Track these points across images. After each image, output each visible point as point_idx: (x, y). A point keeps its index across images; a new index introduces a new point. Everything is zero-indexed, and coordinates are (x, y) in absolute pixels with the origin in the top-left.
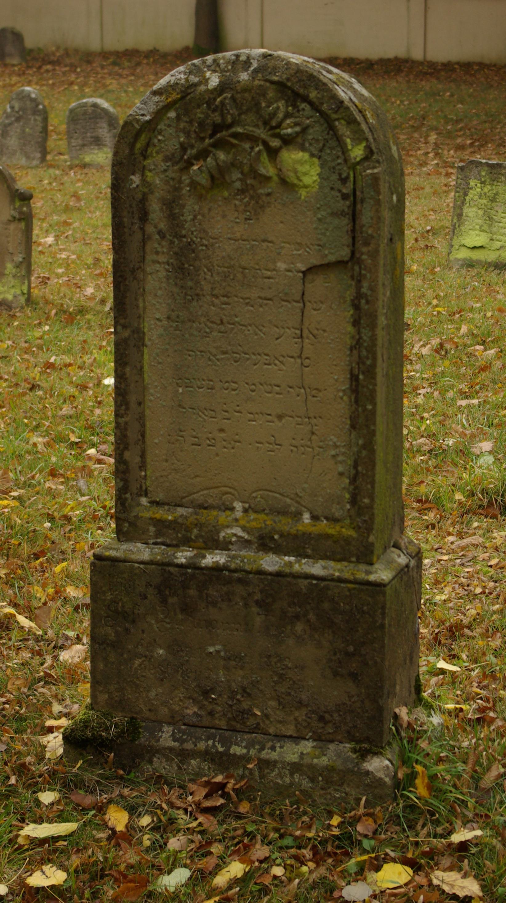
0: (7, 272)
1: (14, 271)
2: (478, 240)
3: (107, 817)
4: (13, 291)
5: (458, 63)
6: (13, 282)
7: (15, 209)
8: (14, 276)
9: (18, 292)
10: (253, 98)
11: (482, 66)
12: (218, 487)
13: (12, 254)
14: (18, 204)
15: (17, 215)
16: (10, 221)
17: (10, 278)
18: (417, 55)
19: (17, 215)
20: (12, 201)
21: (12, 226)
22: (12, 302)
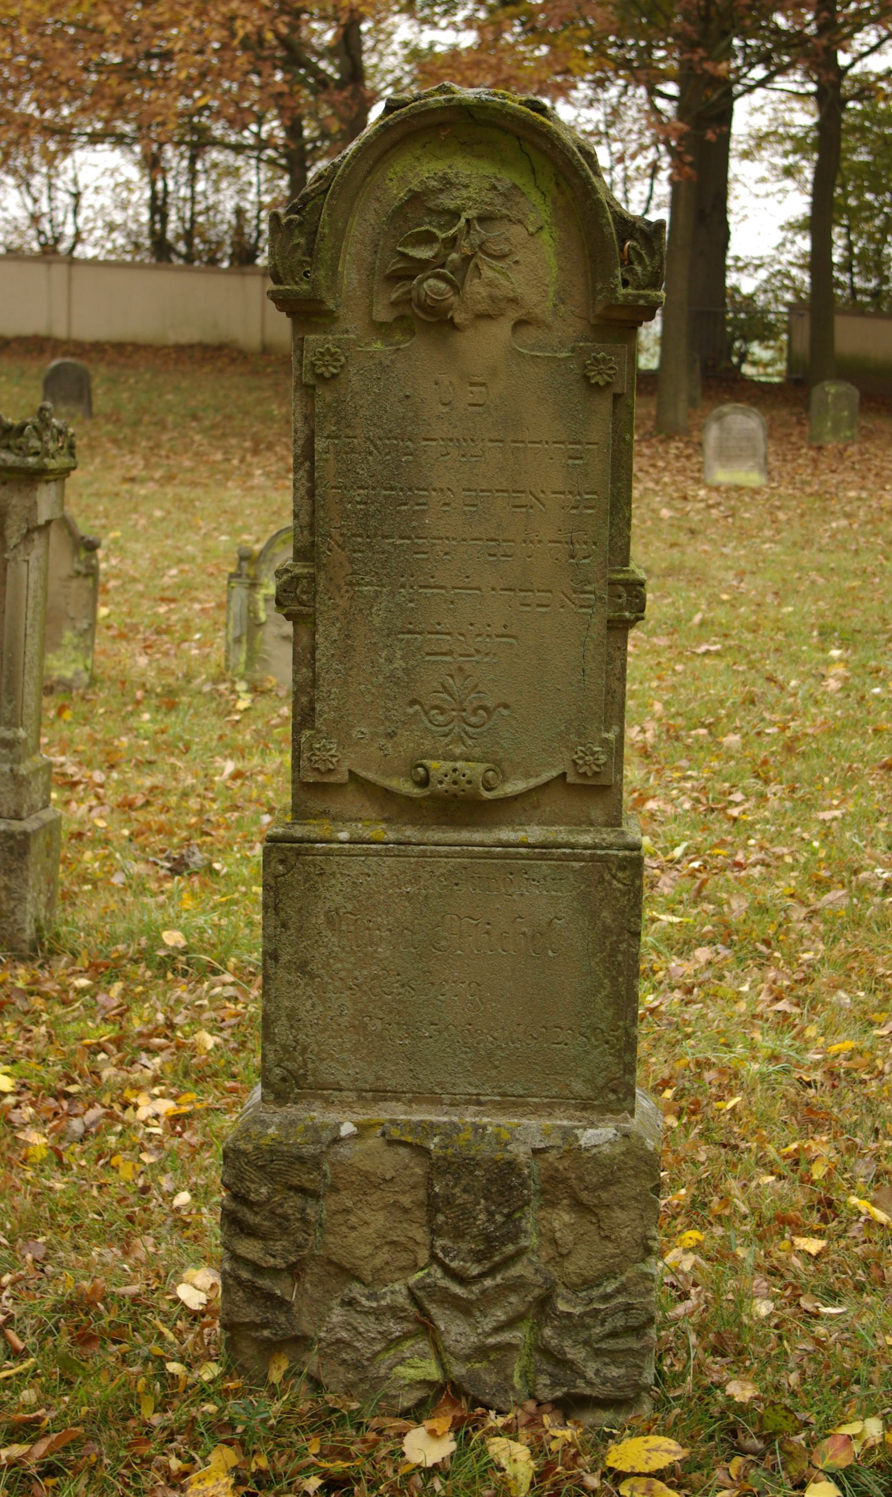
0: (65, 641)
1: (76, 641)
2: (732, 544)
3: (625, 828)
4: (73, 667)
5: (108, 343)
6: (74, 655)
7: (79, 561)
8: (76, 648)
9: (81, 667)
10: (573, 350)
11: (138, 347)
12: (410, 843)
13: (72, 619)
14: (83, 555)
15: (83, 570)
16: (71, 577)
17: (70, 649)
18: (60, 331)
19: (83, 570)
20: (75, 552)
21: (75, 584)
22: (72, 680)
